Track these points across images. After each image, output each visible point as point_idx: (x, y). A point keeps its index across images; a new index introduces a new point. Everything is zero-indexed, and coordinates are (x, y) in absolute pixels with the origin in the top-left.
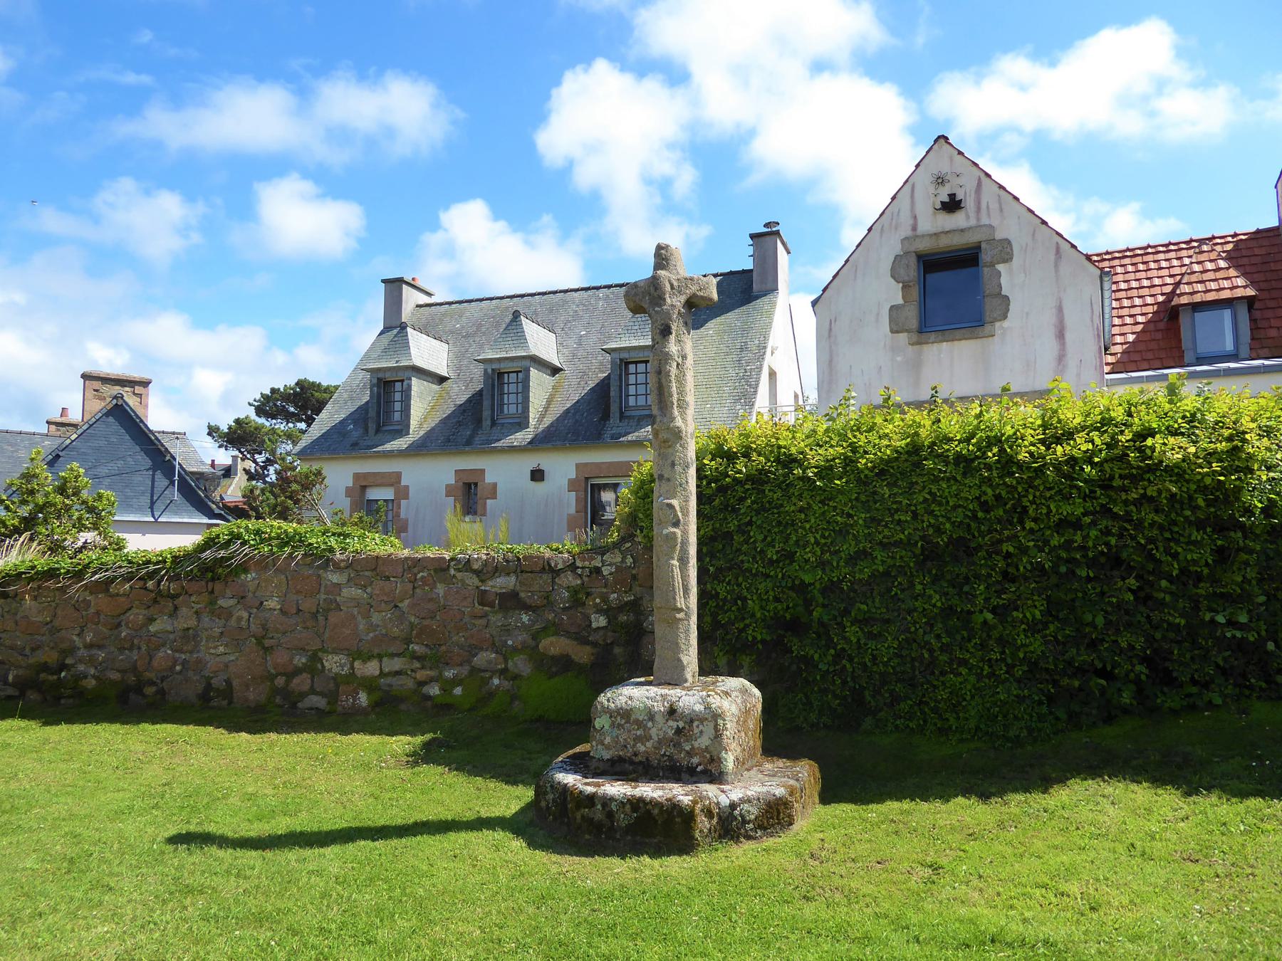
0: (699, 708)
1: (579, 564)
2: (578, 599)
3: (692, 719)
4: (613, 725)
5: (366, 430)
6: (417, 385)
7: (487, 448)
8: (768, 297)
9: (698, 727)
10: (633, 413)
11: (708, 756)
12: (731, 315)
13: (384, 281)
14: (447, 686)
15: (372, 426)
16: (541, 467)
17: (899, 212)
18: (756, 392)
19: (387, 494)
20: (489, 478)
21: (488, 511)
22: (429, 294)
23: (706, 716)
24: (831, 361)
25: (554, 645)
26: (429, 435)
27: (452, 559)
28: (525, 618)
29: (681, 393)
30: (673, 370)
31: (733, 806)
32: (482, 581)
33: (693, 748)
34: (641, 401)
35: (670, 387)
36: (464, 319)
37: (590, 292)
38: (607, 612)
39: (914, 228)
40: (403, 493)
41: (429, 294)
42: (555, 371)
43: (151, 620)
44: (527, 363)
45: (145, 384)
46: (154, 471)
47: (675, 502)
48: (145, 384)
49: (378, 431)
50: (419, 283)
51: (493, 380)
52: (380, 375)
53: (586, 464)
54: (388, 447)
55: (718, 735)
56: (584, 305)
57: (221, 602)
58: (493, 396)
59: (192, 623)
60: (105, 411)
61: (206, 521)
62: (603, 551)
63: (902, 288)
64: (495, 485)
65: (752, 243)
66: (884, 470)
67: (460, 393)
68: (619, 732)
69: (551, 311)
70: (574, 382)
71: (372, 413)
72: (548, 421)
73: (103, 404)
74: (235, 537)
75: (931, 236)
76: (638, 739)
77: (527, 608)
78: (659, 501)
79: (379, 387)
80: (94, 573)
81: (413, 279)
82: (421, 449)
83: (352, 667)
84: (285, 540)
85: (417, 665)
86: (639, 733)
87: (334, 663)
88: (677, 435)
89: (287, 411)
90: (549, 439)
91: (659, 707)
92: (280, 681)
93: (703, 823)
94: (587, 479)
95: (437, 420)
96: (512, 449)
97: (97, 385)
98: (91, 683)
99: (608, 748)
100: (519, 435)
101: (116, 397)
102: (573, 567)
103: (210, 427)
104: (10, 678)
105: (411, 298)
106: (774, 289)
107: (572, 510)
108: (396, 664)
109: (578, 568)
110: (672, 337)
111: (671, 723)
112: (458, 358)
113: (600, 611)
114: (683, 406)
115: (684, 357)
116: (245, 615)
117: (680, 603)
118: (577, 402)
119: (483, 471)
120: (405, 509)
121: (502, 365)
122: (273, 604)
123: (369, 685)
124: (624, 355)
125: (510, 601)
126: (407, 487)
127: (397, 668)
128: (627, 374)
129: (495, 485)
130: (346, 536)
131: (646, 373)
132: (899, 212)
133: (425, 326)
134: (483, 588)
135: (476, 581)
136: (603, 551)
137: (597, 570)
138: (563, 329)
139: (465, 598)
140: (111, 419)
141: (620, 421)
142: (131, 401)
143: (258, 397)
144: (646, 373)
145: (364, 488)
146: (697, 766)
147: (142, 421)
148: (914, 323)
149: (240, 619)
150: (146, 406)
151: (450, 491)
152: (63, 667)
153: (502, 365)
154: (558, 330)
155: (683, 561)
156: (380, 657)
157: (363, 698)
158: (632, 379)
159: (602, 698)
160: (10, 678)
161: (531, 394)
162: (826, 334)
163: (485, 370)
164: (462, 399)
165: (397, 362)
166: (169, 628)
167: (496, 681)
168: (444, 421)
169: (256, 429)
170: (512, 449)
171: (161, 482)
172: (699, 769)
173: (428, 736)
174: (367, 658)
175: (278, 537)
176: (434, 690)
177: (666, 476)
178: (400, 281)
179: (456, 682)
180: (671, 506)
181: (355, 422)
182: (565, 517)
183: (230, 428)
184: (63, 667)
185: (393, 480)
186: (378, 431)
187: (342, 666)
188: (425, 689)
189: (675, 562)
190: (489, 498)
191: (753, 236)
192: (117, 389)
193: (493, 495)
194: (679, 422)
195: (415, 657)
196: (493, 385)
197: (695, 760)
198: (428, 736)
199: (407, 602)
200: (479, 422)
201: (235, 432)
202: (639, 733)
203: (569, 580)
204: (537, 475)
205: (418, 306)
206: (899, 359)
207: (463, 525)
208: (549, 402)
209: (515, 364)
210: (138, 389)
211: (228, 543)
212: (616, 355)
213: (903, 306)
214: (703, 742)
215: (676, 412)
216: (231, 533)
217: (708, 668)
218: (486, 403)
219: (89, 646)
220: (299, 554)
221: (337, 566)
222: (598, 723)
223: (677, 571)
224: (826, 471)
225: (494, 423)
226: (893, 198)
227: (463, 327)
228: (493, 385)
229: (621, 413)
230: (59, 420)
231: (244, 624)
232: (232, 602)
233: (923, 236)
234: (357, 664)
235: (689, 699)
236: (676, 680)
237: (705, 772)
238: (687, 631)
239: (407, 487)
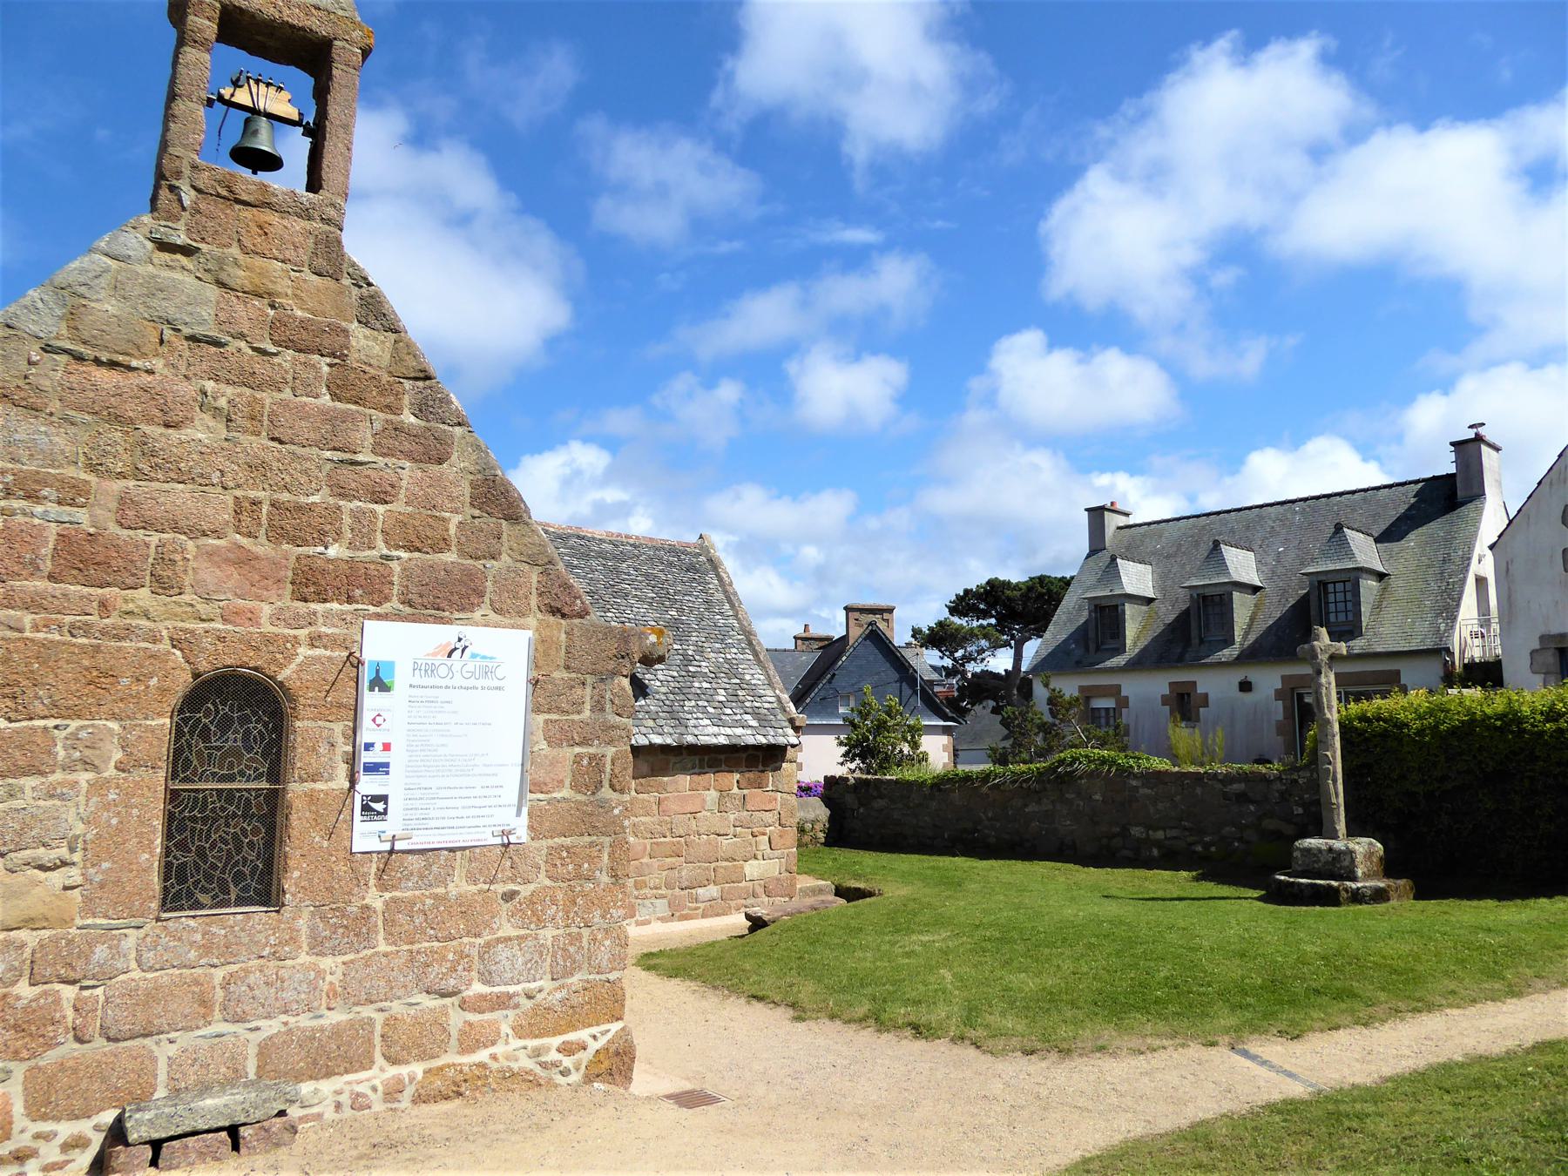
0: (1343, 848)
1: (1284, 777)
2: (1284, 796)
3: (1340, 853)
4: (1302, 855)
5: (1087, 649)
6: (1129, 610)
7: (1196, 663)
8: (1474, 503)
12: (1433, 525)
13: (1086, 510)
14: (1206, 846)
15: (1092, 646)
16: (1249, 679)
18: (1458, 605)
19: (1108, 703)
20: (1200, 690)
21: (1201, 717)
22: (1127, 515)
24: (1509, 597)
25: (1270, 824)
26: (1144, 651)
27: (1205, 773)
28: (1252, 808)
29: (1329, 701)
30: (1324, 691)
32: (1225, 786)
34: (1342, 617)
36: (1163, 539)
37: (1286, 507)
38: (1304, 805)
40: (1123, 702)
41: (1127, 515)
42: (1255, 589)
43: (1026, 805)
44: (1229, 588)
45: (890, 610)
46: (901, 683)
47: (1328, 753)
48: (890, 610)
49: (1098, 649)
50: (1119, 507)
51: (1199, 603)
52: (1098, 602)
53: (1290, 676)
54: (1109, 663)
55: (1353, 861)
56: (1281, 521)
57: (1067, 796)
59: (1051, 807)
60: (864, 636)
61: (942, 723)
62: (1298, 769)
64: (1206, 695)
66: (1453, 731)
67: (1168, 614)
69: (1248, 528)
70: (1275, 599)
71: (1091, 634)
72: (1252, 638)
73: (862, 630)
74: (1075, 760)
76: (1315, 862)
77: (1252, 802)
78: (1320, 752)
79: (1096, 612)
80: (994, 780)
81: (1112, 504)
82: (1137, 665)
83: (1148, 834)
84: (1103, 761)
85: (1187, 833)
87: (1137, 831)
88: (1328, 722)
89: (979, 608)
90: (1254, 655)
91: (1324, 848)
92: (1105, 841)
93: (1344, 894)
94: (1293, 689)
95: (1150, 639)
96: (1220, 664)
97: (857, 615)
98: (992, 840)
99: (1300, 865)
100: (1226, 652)
101: (870, 624)
102: (1279, 778)
103: (914, 630)
104: (946, 836)
105: (1112, 522)
106: (1481, 494)
107: (1280, 717)
108: (1174, 833)
110: (1323, 675)
112: (1161, 580)
113: (1298, 805)
114: (1330, 708)
115: (1330, 684)
116: (1082, 804)
117: (1334, 800)
118: (1280, 618)
120: (1126, 717)
121: (1206, 590)
122: (1098, 797)
123: (1158, 844)
124: (1322, 578)
125: (1242, 798)
126: (1127, 698)
127: (1175, 835)
128: (1326, 593)
129: (1206, 695)
130: (1139, 759)
131: (1335, 592)
133: (1128, 548)
135: (1220, 786)
136: (1298, 769)
138: (1261, 546)
140: (868, 642)
142: (882, 625)
143: (954, 598)
144: (1345, 602)
145: (1088, 699)
147: (890, 642)
149: (1078, 805)
150: (892, 629)
151: (1165, 700)
152: (976, 830)
153: (1206, 590)
154: (1256, 547)
155: (1335, 781)
156: (1164, 829)
157: (1155, 852)
158: (1331, 598)
159: (1297, 844)
160: (946, 836)
161: (1235, 615)
163: (1191, 596)
164: (1171, 618)
165: (1111, 591)
166: (1037, 810)
167: (1236, 844)
168: (1154, 639)
169: (957, 630)
170: (1220, 664)
171: (907, 691)
173: (1200, 871)
174: (1156, 829)
175: (1099, 759)
176: (1199, 848)
178: (1102, 509)
179: (1212, 844)
180: (1327, 756)
181: (1076, 642)
182: (1274, 723)
183: (930, 629)
184: (976, 830)
185: (1115, 691)
186: (1098, 649)
187: (1142, 833)
188: (1193, 847)
189: (1330, 782)
192: (871, 618)
193: (1206, 705)
194: (1328, 715)
195: (1186, 829)
196: (1199, 608)
198: (1200, 871)
199: (1179, 797)
200: (1187, 641)
201: (937, 633)
203: (1278, 786)
204: (1245, 686)
205: (1120, 528)
207: (1177, 730)
208: (1252, 619)
209: (1218, 589)
210: (886, 616)
211: (1071, 764)
212: (1314, 578)
214: (1346, 863)
215: (1326, 711)
216: (1072, 757)
217: (1351, 833)
218: (1194, 624)
219: (989, 819)
220: (1114, 769)
221: (1135, 776)
222: (1295, 854)
223: (1331, 786)
224: (1420, 732)
225: (1202, 641)
226: (1560, 456)
227: (1163, 548)
228: (1199, 608)
230: (804, 635)
231: (1081, 808)
232: (1073, 796)
234: (1150, 832)
235: (1339, 845)
236: (1335, 837)
238: (1339, 815)
239: (1127, 698)
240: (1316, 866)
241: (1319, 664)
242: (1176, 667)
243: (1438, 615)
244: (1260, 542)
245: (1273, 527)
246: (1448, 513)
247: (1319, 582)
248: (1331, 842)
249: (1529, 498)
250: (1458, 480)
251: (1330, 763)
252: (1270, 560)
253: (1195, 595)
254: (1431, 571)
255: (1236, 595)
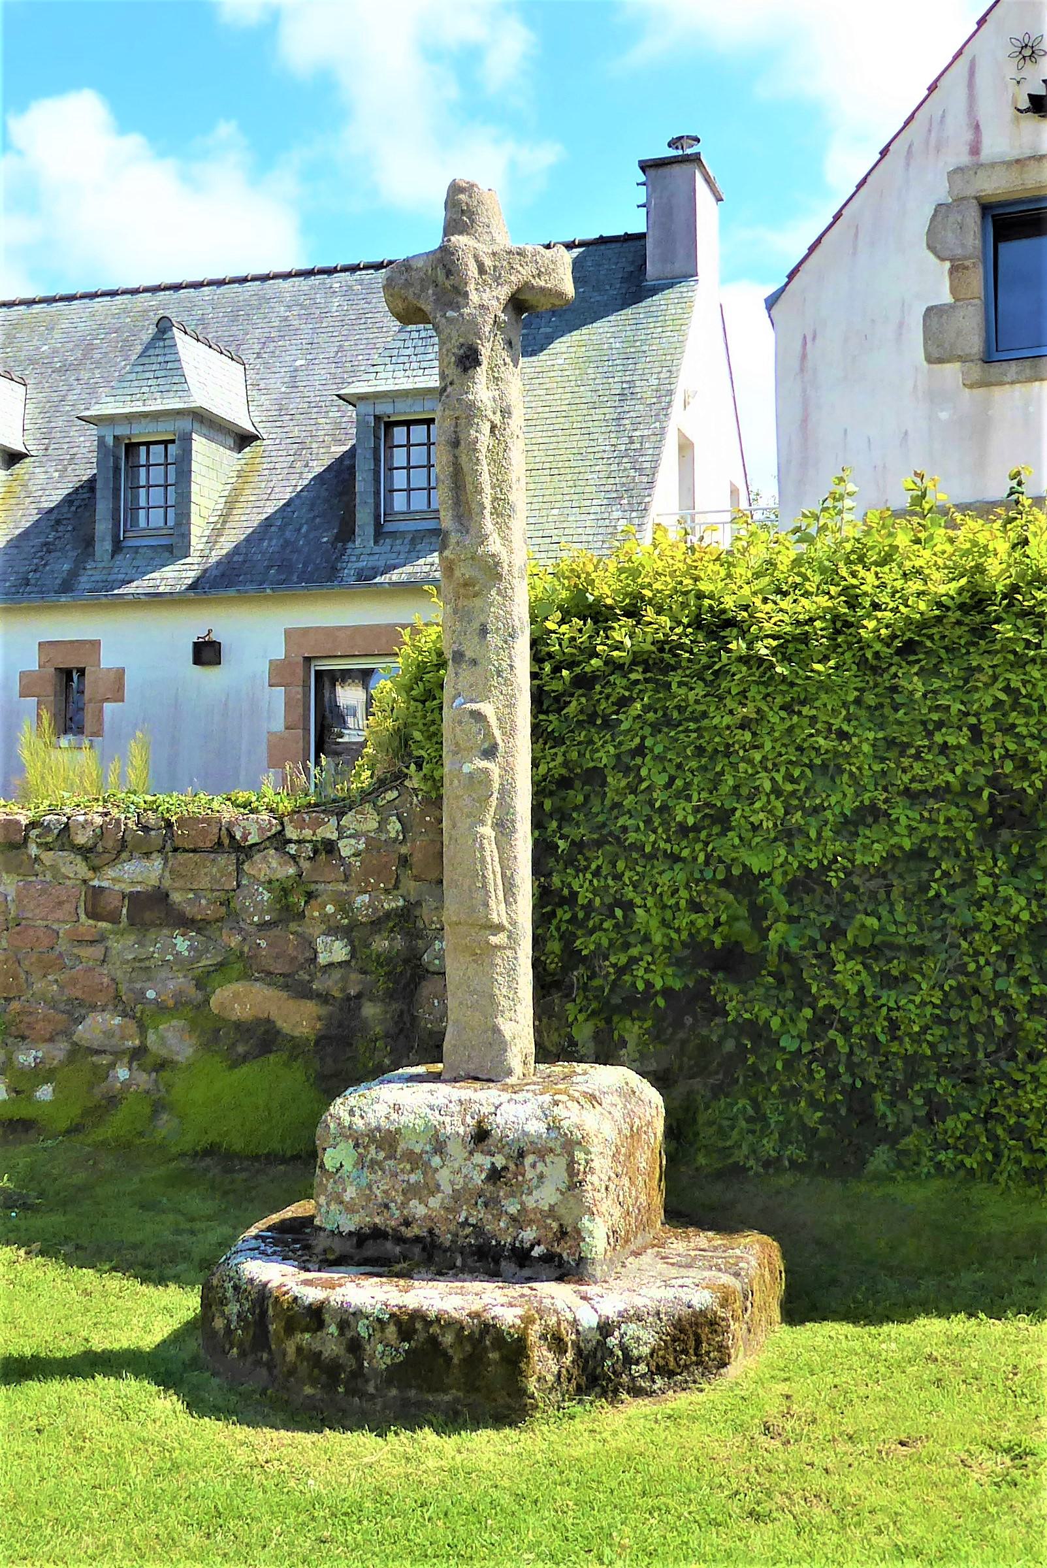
0: (536, 1127)
1: (291, 833)
4: (360, 1162)
8: (676, 289)
9: (534, 1166)
10: (402, 526)
11: (555, 1225)
16: (213, 637)
17: (943, 117)
20: (108, 660)
21: (106, 726)
23: (551, 1144)
24: (805, 420)
28: (182, 944)
31: (605, 1329)
33: (523, 1210)
35: (476, 473)
36: (57, 334)
39: (975, 150)
44: (184, 424)
51: (117, 459)
58: (116, 490)
60: (129, 889)
62: (340, 808)
63: (951, 272)
64: (120, 673)
65: (643, 178)
68: (372, 1177)
70: (283, 463)
72: (226, 545)
75: (1008, 164)
76: (411, 1191)
77: (185, 923)
86: (413, 1178)
88: (492, 571)
94: (308, 660)
96: (156, 599)
99: (350, 1209)
106: (690, 274)
109: (290, 841)
110: (481, 373)
111: (479, 1158)
113: (333, 931)
115: (506, 412)
119: (95, 645)
124: (384, 408)
129: (120, 673)
132: (943, 117)
134: (96, 883)
135: (81, 868)
136: (340, 808)
137: (330, 847)
139: (61, 903)
141: (376, 542)
146: (532, 1247)
148: (974, 343)
155: (504, 827)
158: (399, 458)
159: (339, 1108)
162: (795, 363)
163: (101, 441)
167: (122, 1073)
170: (156, 599)
172: (537, 1251)
177: (469, 654)
180: (478, 716)
182: (264, 738)
190: (107, 700)
191: (646, 166)
193: (117, 694)
196: (117, 469)
197: (529, 1235)
202: (413, 1178)
206: (944, 415)
208: (231, 504)
209: (161, 427)
212: (367, 408)
213: (951, 306)
214: (545, 1196)
215: (489, 524)
225: (118, 547)
226: (932, 88)
228: (117, 469)
229: (378, 527)
233: (993, 165)
237: (549, 1258)
240: (418, 1209)
241: (473, 327)
242: (55, 607)
243: (615, 500)
244: (257, 348)
245: (286, 319)
246: (625, 305)
247: (377, 418)
248: (484, 1097)
249: (860, 186)
250: (650, 243)
251: (490, 752)
252: (277, 384)
253: (110, 441)
254: (598, 414)
255: (200, 444)
